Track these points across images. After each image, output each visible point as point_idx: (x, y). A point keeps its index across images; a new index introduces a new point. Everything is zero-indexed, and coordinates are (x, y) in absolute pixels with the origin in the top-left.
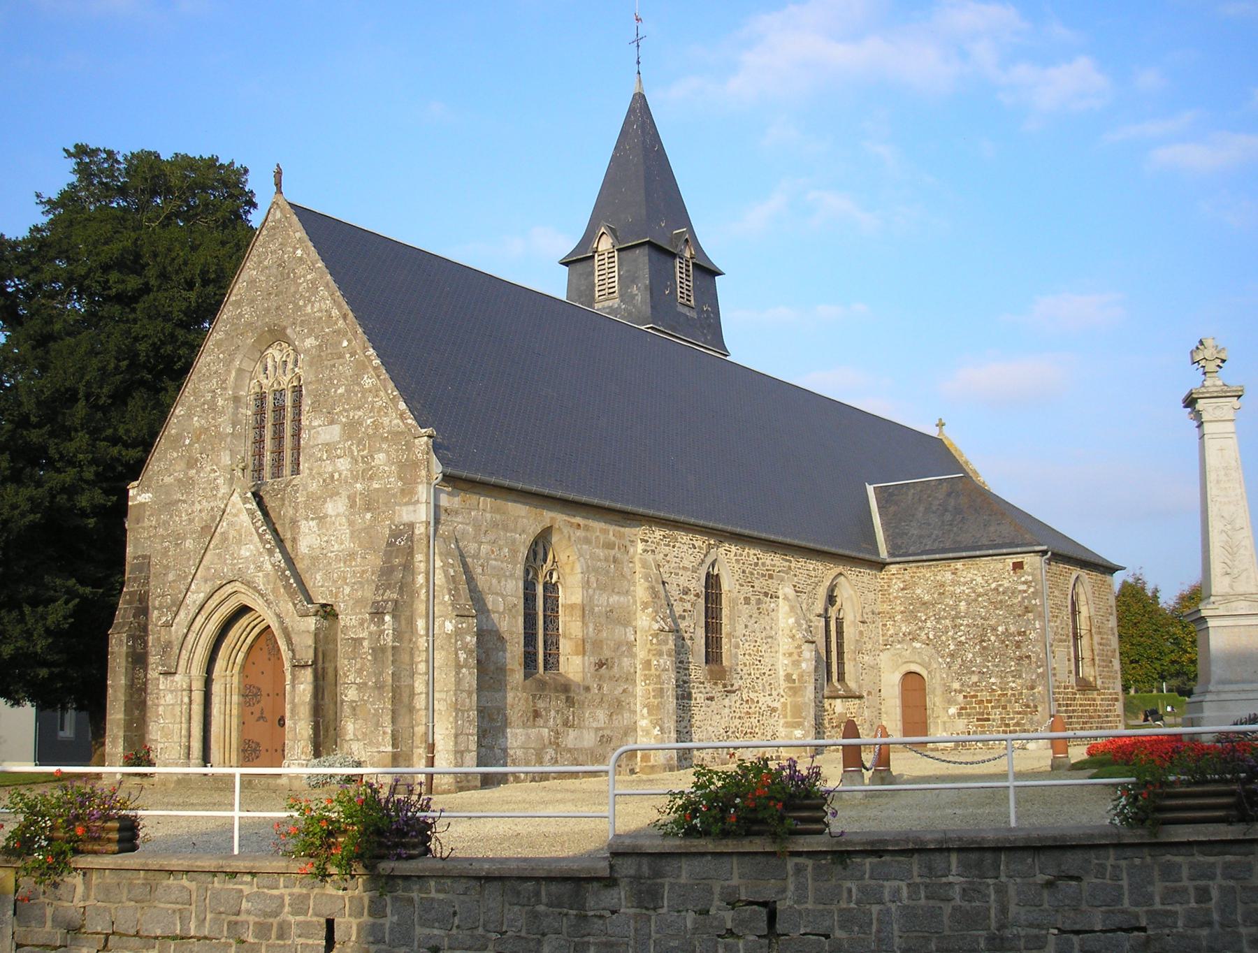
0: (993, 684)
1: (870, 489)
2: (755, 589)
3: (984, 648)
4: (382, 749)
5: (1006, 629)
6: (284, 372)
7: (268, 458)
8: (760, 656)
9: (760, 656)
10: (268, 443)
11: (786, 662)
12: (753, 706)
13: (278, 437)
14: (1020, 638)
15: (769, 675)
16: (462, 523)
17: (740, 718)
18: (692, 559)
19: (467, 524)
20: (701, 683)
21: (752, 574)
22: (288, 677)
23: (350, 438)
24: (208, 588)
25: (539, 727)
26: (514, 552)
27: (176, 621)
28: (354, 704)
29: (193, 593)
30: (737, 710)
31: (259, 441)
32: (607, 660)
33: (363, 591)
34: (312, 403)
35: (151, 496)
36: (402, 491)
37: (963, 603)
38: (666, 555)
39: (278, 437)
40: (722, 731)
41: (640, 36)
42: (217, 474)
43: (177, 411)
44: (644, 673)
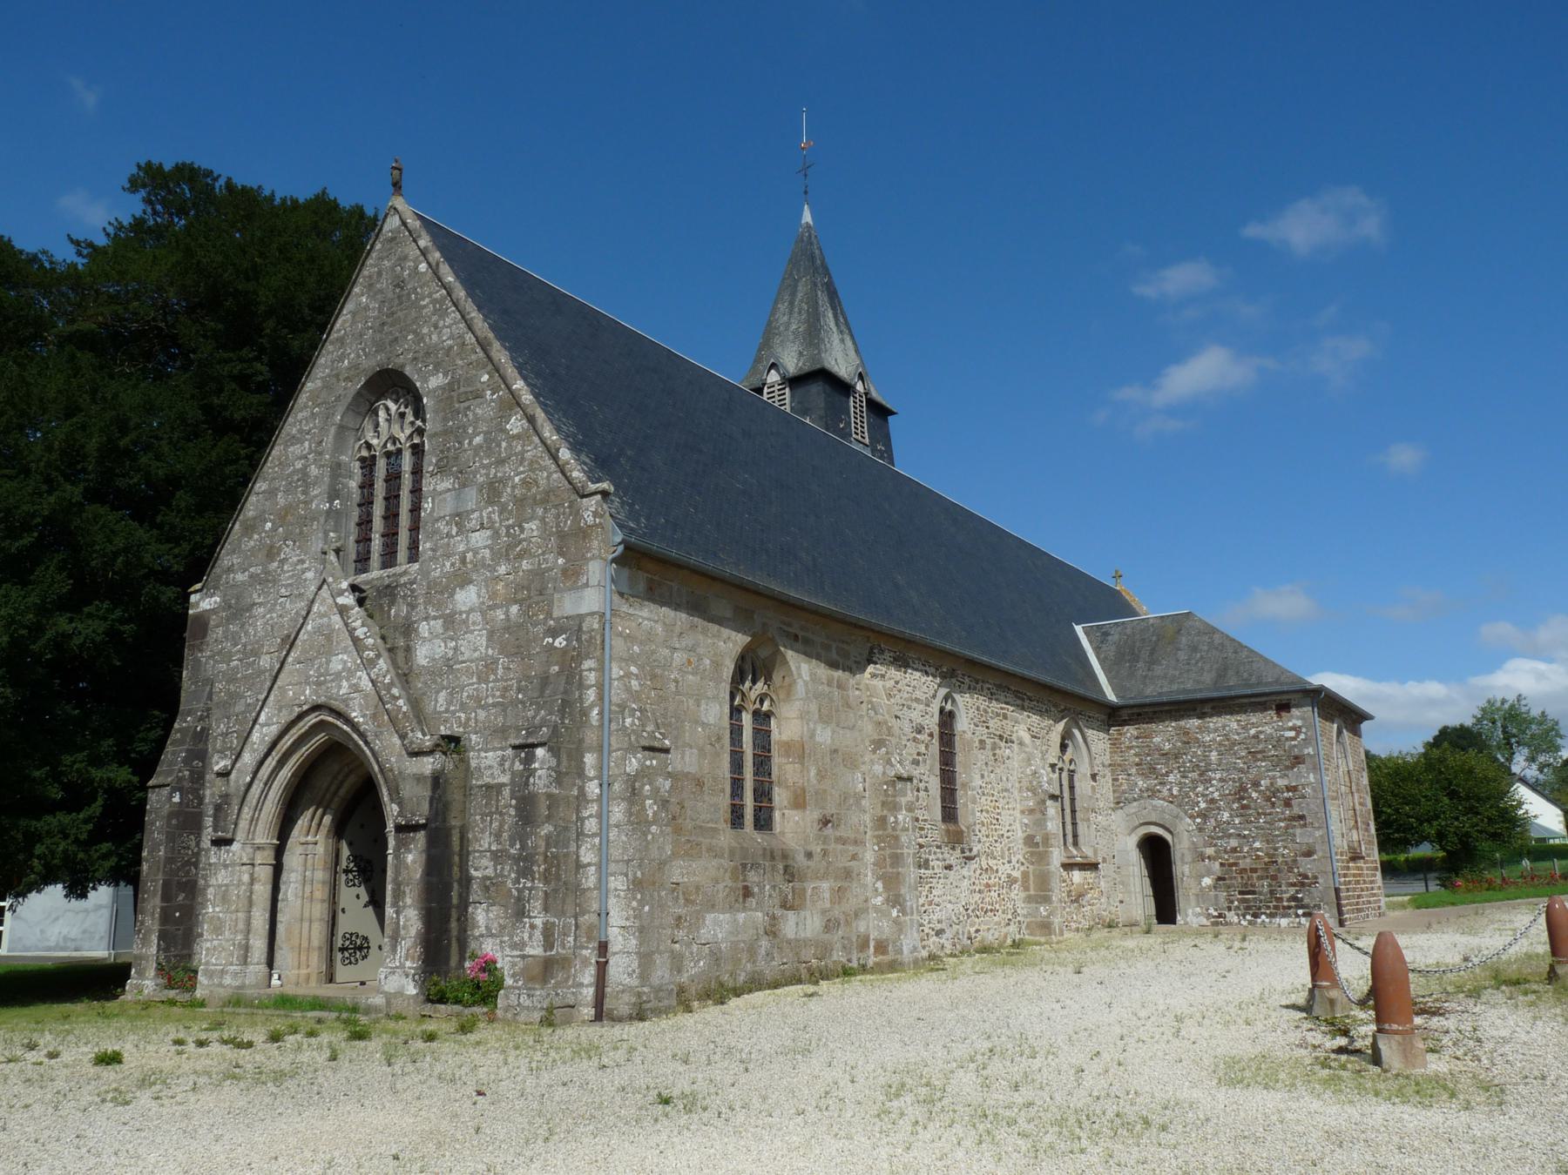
0: (1258, 850)
1: (1079, 629)
2: (991, 730)
3: (1244, 807)
4: (529, 951)
5: (1272, 784)
6: (402, 428)
7: (377, 543)
8: (998, 814)
9: (998, 814)
10: (378, 524)
11: (1026, 821)
12: (993, 877)
13: (391, 516)
14: (1291, 794)
15: (1008, 838)
16: (649, 619)
17: (980, 892)
18: (925, 689)
19: (656, 622)
20: (938, 847)
21: (986, 712)
22: (391, 842)
23: (490, 502)
24: (285, 717)
25: (751, 910)
26: (717, 665)
27: (238, 765)
28: (488, 883)
29: (262, 726)
30: (977, 882)
31: (365, 523)
32: (832, 816)
33: (505, 717)
34: (438, 461)
35: (218, 599)
36: (565, 571)
37: (1214, 753)
38: (897, 683)
39: (391, 516)
40: (962, 909)
41: (807, 165)
42: (306, 566)
43: (258, 485)
44: (876, 833)
